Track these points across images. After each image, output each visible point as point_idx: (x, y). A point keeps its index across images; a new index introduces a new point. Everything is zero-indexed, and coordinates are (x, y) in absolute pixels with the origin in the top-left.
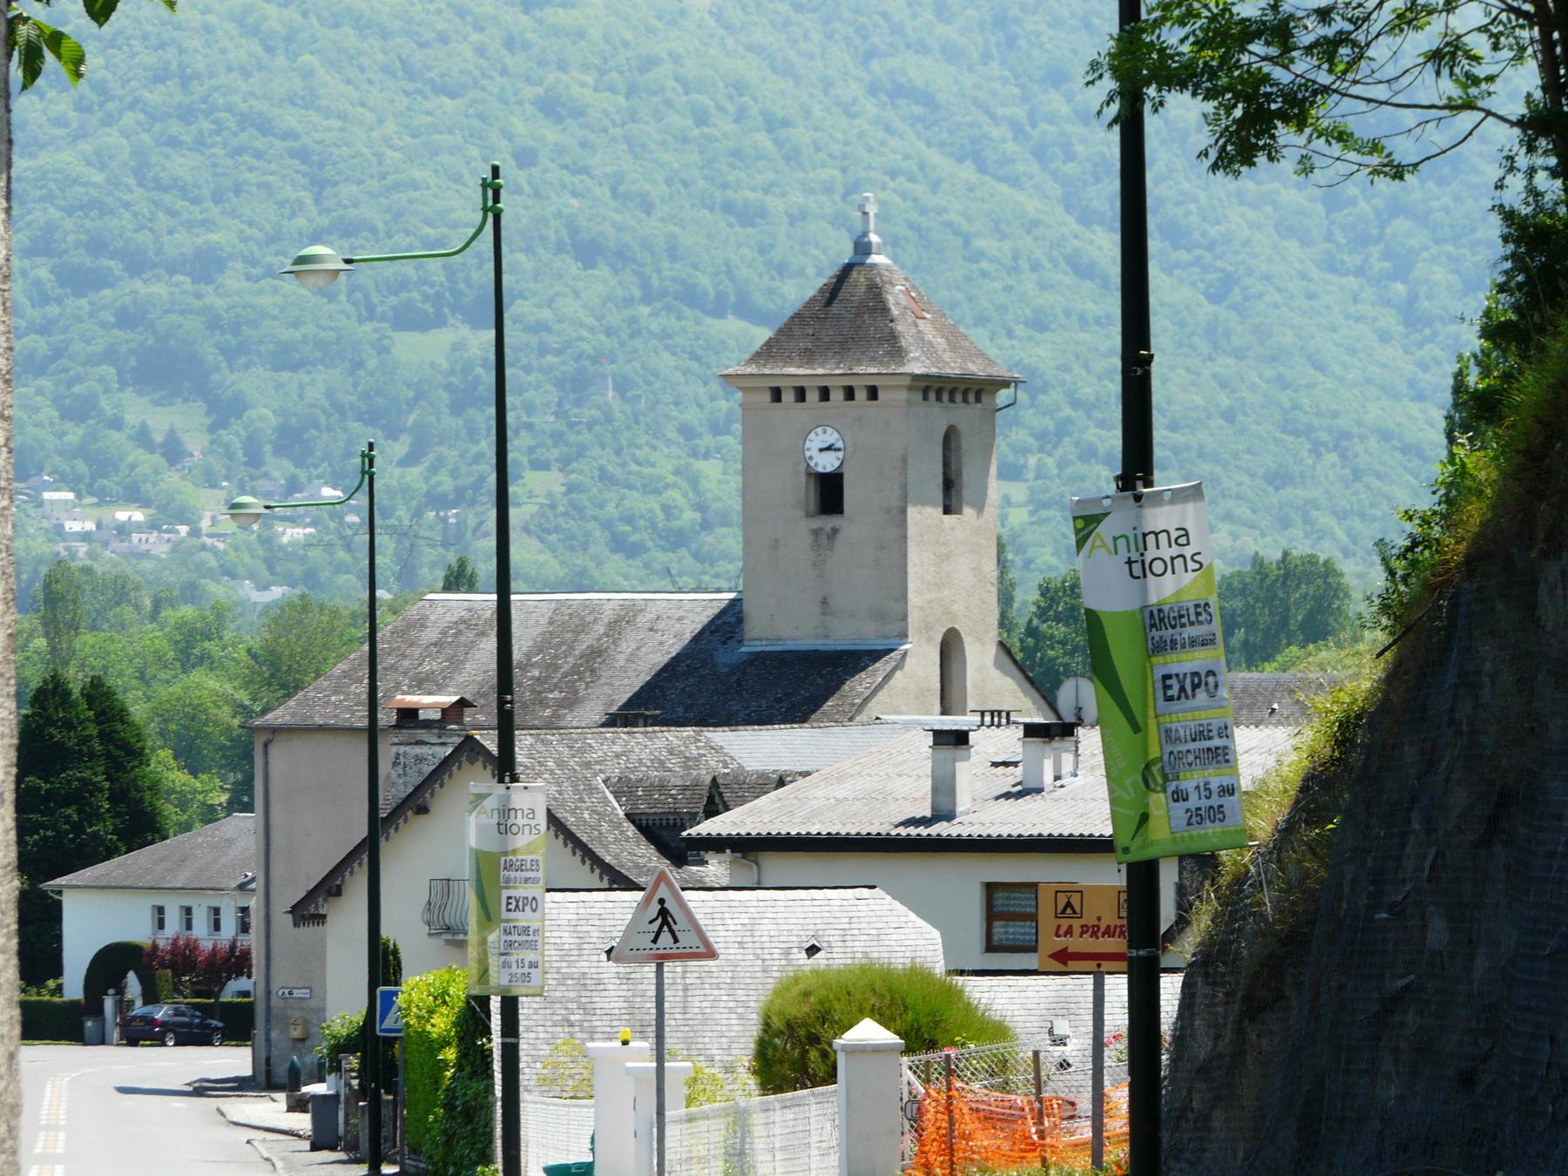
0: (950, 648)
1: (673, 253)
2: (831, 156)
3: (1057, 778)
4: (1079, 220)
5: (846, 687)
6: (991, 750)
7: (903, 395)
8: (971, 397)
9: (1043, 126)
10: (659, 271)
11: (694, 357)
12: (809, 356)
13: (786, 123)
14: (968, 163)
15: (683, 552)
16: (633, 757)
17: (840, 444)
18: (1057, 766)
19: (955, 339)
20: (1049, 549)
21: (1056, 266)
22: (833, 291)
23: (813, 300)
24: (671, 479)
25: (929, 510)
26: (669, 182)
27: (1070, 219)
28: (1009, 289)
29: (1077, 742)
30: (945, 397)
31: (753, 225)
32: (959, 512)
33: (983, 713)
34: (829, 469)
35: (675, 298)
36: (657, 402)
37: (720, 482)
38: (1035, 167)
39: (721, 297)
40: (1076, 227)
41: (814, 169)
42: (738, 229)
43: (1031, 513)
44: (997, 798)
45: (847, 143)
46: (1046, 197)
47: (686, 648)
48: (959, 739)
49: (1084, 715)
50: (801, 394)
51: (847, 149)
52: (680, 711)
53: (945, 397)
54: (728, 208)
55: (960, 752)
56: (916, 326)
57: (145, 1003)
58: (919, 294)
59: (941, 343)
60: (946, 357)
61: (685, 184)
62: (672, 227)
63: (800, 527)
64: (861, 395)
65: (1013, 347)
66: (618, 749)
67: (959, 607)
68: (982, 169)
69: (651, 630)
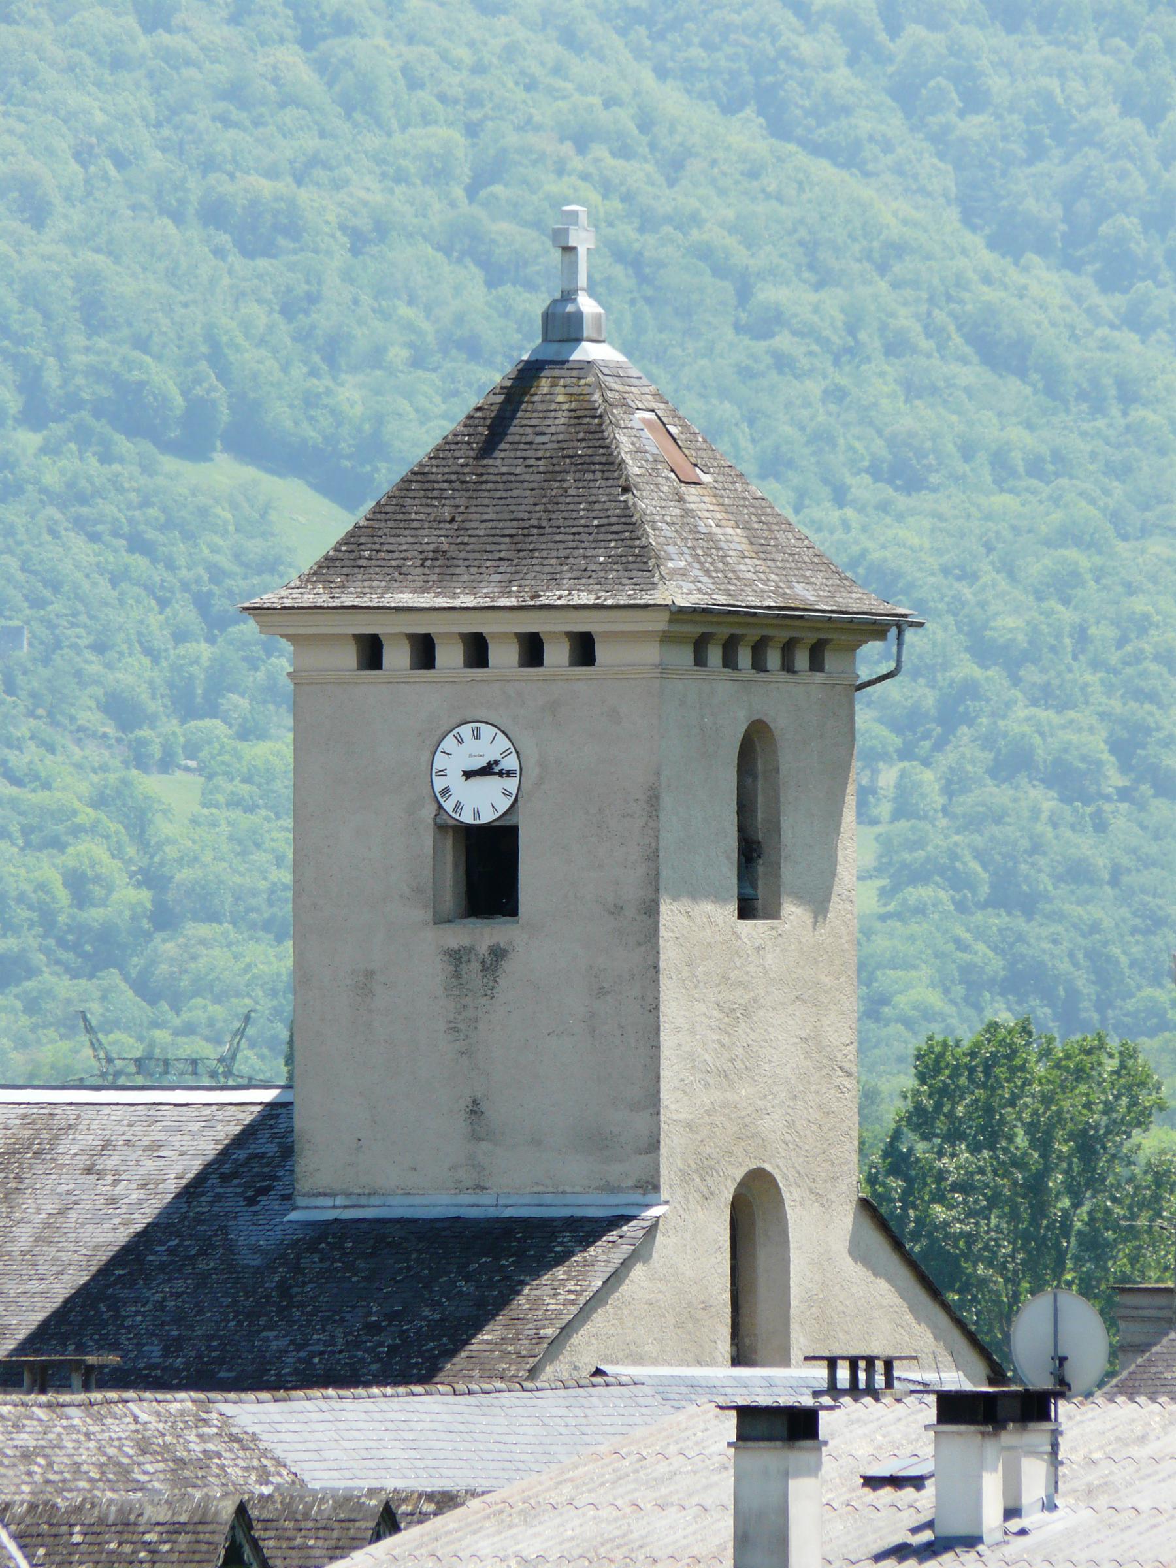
0: (753, 1215)
1: (93, 313)
2: (442, 98)
3: (1011, 1513)
4: (993, 244)
5: (522, 1301)
6: (863, 1450)
7: (651, 653)
8: (802, 660)
9: (914, 32)
10: (60, 353)
11: (138, 544)
12: (441, 566)
13: (344, 26)
14: (749, 112)
15: (112, 977)
16: (60, 1459)
17: (511, 763)
18: (1012, 1485)
19: (763, 529)
20: (925, 972)
21: (940, 347)
22: (498, 421)
23: (449, 444)
24: (87, 815)
25: (708, 907)
26: (83, 155)
27: (975, 241)
28: (836, 394)
29: (1056, 1434)
30: (744, 657)
31: (269, 250)
32: (773, 913)
33: (832, 1363)
34: (487, 817)
35: (98, 414)
36: (58, 645)
37: (195, 822)
38: (895, 125)
39: (198, 415)
40: (988, 258)
41: (404, 128)
42: (236, 260)
43: (885, 894)
44: (878, 1557)
45: (479, 69)
46: (923, 191)
47: (169, 1210)
48: (796, 1426)
49: (1072, 1373)
50: (424, 651)
51: (478, 82)
52: (155, 1351)
53: (744, 657)
54: (214, 214)
55: (799, 1455)
56: (681, 500)
58: (685, 428)
59: (734, 538)
60: (746, 569)
61: (121, 162)
62: (91, 256)
63: (419, 943)
64: (557, 654)
65: (846, 525)
66: (25, 1439)
67: (771, 1125)
68: (779, 128)
69: (89, 1170)
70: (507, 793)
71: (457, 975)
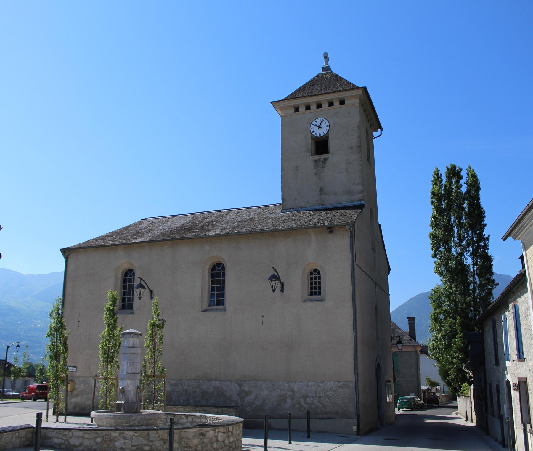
57: (42, 413)
63: (308, 161)
70: (326, 123)
71: (316, 164)
